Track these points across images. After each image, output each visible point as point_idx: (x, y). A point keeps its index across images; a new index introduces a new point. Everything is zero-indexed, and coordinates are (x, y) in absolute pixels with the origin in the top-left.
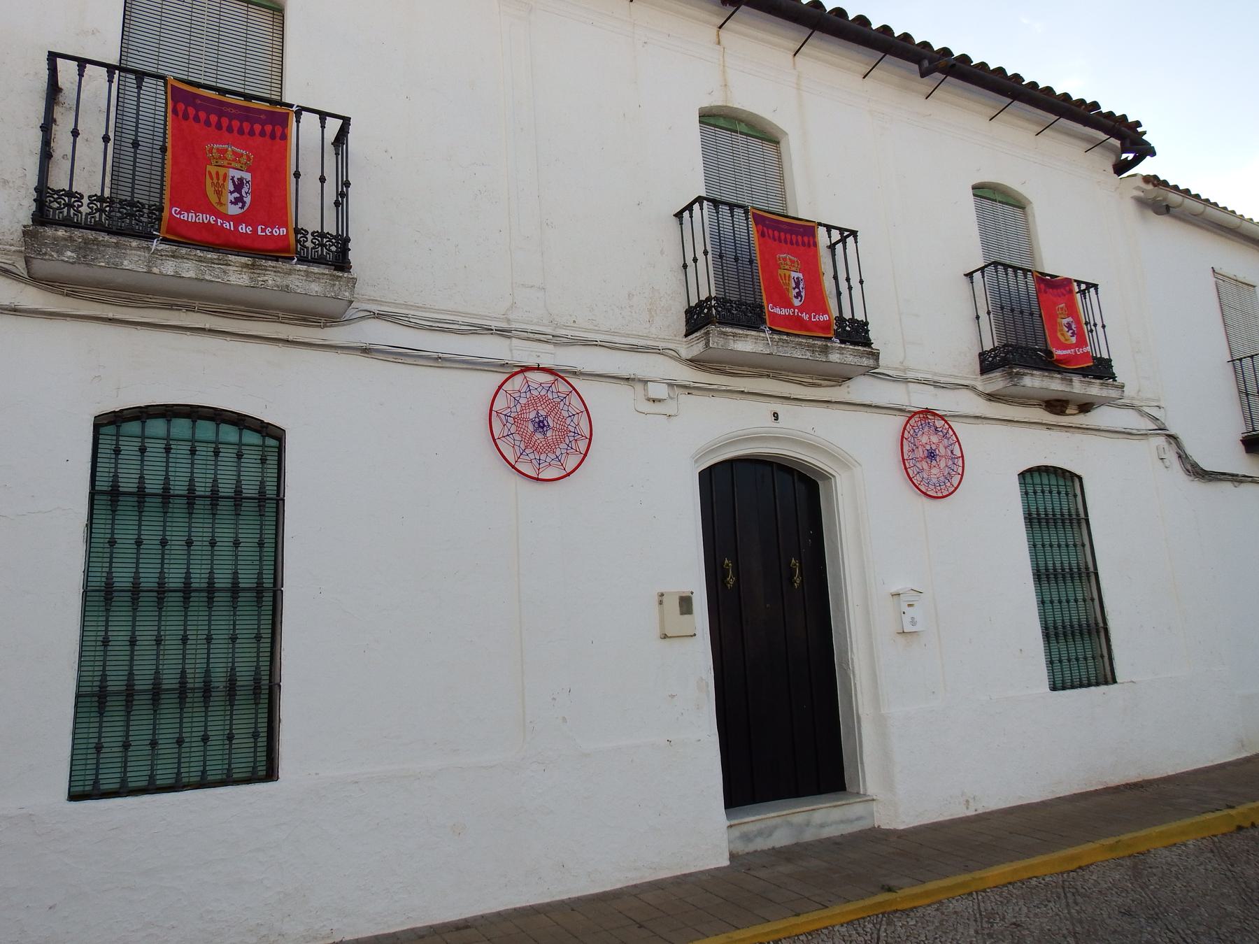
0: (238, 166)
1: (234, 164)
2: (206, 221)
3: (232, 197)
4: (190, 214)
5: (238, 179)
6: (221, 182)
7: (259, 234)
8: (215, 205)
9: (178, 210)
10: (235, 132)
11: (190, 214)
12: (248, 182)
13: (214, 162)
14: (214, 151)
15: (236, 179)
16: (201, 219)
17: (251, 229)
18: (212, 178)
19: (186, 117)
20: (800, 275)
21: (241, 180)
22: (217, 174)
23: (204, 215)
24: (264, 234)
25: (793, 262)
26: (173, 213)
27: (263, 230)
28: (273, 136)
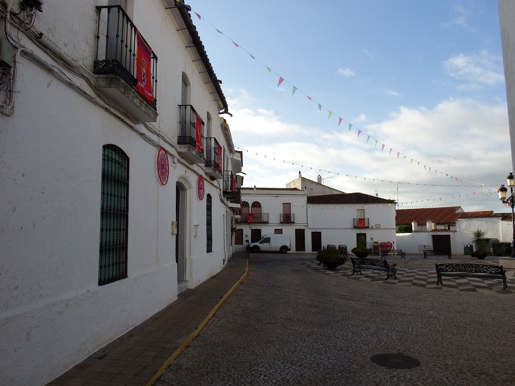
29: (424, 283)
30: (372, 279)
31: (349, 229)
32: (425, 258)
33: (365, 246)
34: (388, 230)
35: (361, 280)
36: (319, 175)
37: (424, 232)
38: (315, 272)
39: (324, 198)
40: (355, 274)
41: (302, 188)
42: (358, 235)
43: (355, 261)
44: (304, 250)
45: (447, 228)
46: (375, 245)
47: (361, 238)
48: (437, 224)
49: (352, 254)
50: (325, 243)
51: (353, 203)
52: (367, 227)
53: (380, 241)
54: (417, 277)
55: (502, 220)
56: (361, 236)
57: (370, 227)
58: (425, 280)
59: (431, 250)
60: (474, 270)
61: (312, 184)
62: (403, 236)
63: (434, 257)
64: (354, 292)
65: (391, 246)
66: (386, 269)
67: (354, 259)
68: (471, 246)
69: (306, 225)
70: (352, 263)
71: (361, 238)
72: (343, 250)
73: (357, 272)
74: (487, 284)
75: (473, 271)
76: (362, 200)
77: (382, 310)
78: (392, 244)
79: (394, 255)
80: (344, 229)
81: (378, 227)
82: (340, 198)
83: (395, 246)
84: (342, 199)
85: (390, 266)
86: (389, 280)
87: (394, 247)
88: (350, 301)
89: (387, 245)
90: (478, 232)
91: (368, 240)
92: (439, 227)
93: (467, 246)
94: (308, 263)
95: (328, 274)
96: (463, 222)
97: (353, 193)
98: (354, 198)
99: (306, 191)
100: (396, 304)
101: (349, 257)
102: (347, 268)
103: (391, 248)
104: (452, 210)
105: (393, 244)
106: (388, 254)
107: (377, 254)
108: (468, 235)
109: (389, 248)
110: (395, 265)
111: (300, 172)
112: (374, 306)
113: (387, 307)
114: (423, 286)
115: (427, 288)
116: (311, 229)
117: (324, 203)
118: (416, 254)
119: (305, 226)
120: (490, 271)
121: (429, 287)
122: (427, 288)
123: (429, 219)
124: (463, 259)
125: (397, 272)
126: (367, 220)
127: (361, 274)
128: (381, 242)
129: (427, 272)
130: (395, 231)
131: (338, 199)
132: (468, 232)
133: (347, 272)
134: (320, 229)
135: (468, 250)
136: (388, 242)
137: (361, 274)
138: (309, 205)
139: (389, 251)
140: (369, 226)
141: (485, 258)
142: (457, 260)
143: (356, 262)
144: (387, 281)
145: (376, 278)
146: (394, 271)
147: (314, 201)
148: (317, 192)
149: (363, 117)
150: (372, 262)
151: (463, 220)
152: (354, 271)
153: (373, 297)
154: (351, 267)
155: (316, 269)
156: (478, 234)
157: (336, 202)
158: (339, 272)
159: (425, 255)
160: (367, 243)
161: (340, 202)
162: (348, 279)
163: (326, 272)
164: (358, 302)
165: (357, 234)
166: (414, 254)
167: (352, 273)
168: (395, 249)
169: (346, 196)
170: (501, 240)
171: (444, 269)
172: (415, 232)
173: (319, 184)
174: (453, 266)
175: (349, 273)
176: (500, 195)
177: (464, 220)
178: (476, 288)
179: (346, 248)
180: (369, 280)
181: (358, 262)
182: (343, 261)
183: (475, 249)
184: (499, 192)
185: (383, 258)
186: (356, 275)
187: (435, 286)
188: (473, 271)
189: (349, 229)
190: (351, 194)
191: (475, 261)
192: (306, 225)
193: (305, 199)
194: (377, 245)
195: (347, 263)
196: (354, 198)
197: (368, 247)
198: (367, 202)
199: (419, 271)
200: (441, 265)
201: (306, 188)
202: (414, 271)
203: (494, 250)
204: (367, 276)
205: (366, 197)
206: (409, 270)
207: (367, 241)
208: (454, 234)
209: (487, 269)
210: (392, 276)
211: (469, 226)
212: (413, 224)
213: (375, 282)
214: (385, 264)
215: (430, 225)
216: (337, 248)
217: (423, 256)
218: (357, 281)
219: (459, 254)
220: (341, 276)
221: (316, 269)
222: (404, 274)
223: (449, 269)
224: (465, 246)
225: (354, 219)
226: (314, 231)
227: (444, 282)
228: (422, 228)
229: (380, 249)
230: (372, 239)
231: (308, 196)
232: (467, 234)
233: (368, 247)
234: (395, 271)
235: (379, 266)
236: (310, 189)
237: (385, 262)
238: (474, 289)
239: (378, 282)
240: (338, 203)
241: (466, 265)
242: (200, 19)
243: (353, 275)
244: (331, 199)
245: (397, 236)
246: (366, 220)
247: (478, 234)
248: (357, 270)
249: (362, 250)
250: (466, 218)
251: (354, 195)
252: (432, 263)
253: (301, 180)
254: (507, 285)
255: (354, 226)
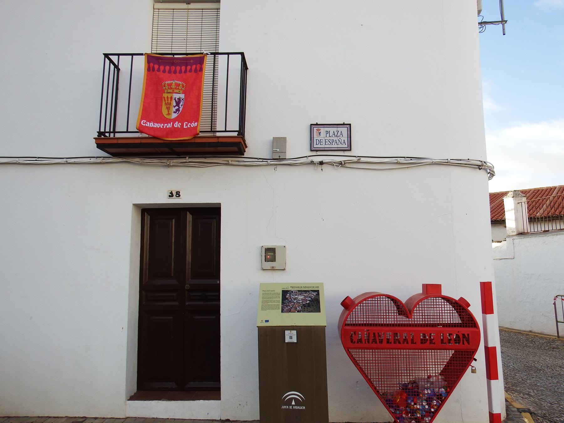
0: (177, 91)
1: (175, 91)
2: (158, 127)
3: (174, 110)
4: (151, 123)
5: (178, 99)
6: (169, 102)
7: (184, 127)
8: (165, 116)
9: (145, 121)
10: (161, 71)
11: (151, 123)
12: (183, 99)
13: (166, 91)
14: (166, 85)
15: (177, 99)
16: (177, 125)
17: (180, 124)
18: (165, 101)
19: (153, 70)
20: (182, 96)
21: (179, 99)
22: (168, 97)
23: (158, 124)
24: (187, 127)
25: (177, 85)
26: (143, 124)
27: (187, 125)
28: (196, 71)
46: (283, 329)
78: (476, 309)
89: (417, 317)
105: (487, 308)
128: (354, 293)
136: (344, 304)
140: (241, 131)
194: (300, 330)
242: (103, 54)
254: (429, 354)
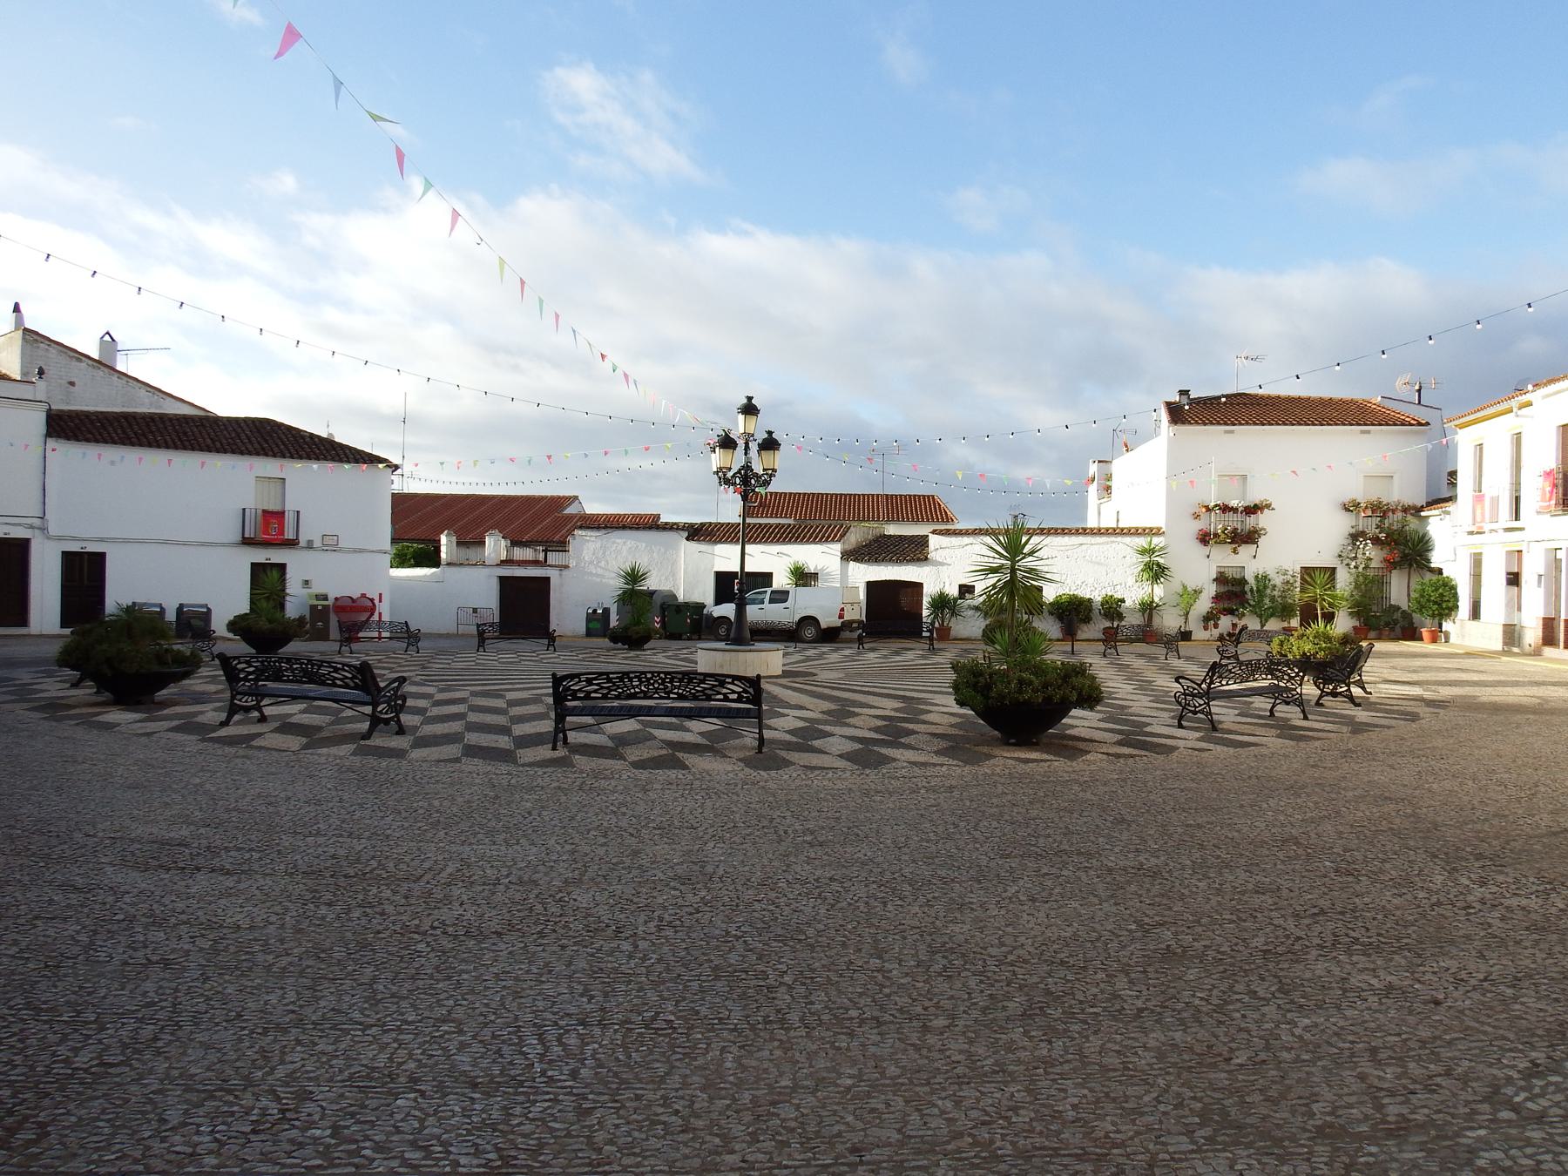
29: (503, 742)
30: (307, 737)
31: (223, 545)
32: (481, 649)
33: (282, 606)
34: (365, 555)
35: (260, 748)
36: (108, 333)
37: (476, 565)
38: (45, 718)
39: (125, 424)
40: (236, 718)
41: (24, 374)
42: (255, 567)
43: (240, 666)
44: (23, 620)
45: (541, 557)
47: (268, 581)
48: (515, 543)
49: (231, 635)
50: (119, 593)
51: (242, 453)
52: (292, 543)
53: (334, 592)
54: (473, 717)
55: (687, 539)
56: (269, 573)
57: (303, 543)
58: (505, 730)
59: (860, 622)
60: (675, 693)
61: (74, 363)
62: (409, 579)
63: (503, 644)
64: (226, 816)
65: (372, 610)
66: (368, 699)
67: (235, 658)
68: (606, 611)
69: (37, 522)
70: (221, 673)
71: (268, 581)
72: (194, 622)
73: (247, 710)
74: (698, 733)
75: (672, 696)
76: (277, 445)
77: (364, 921)
78: (376, 602)
79: (380, 638)
80: (203, 544)
81: (330, 545)
82: (192, 431)
83: (385, 611)
84: (200, 433)
85: (382, 685)
86: (377, 741)
87: (380, 614)
88: (199, 876)
90: (633, 570)
91: (293, 587)
92: (520, 553)
93: (595, 611)
94: (24, 676)
95: (109, 727)
96: (588, 541)
97: (246, 420)
98: (246, 435)
99: (41, 385)
100: (426, 865)
101: (217, 649)
102: (203, 693)
103: (372, 614)
104: (558, 503)
105: (380, 601)
106: (361, 635)
107: (323, 636)
108: (599, 580)
109: (363, 617)
110: (402, 680)
111: (17, 309)
112: (328, 897)
113: (388, 893)
114: (505, 756)
115: (523, 765)
116: (60, 539)
117: (124, 444)
118: (448, 636)
119: (31, 527)
120: (725, 694)
121: (527, 760)
122: (523, 765)
123: (492, 528)
124: (586, 648)
125: (410, 702)
126: (291, 520)
127: (263, 719)
129: (502, 697)
130: (388, 558)
131: (185, 433)
132: (600, 571)
133: (202, 713)
134: (102, 540)
135: (597, 623)
137: (263, 719)
138: (51, 443)
139: (364, 625)
141: (646, 646)
142: (572, 651)
143: (243, 670)
144: (367, 742)
145: (325, 734)
146: (398, 704)
147: (79, 429)
148: (93, 398)
149: (288, 182)
150: (311, 673)
151: (589, 533)
152: (233, 710)
153: (318, 833)
154: (220, 687)
155: (54, 708)
156: (634, 576)
157: (174, 443)
158: (165, 712)
159: (482, 638)
160: (288, 598)
161: (192, 445)
162: (201, 746)
163: (100, 718)
164: (239, 882)
165: (255, 567)
166: (440, 636)
167: (223, 716)
168: (386, 618)
169: (218, 426)
170: (681, 598)
171: (580, 690)
172: (449, 564)
173: (104, 365)
174: (609, 680)
175: (211, 714)
176: (717, 459)
177: (592, 534)
178: (680, 755)
179: (206, 616)
180: (294, 742)
181: (250, 673)
182: (188, 666)
183: (614, 621)
184: (714, 451)
185: (343, 648)
186: (238, 723)
187: (545, 752)
188: (672, 696)
189: (223, 545)
190: (237, 421)
191: (620, 660)
192: (37, 522)
193: (38, 420)
195: (204, 671)
196: (246, 435)
197: (292, 610)
198: (298, 453)
199: (474, 694)
200: (571, 677)
201: (41, 372)
202: (458, 695)
203: (663, 622)
204: (287, 727)
205: (293, 436)
206: (441, 691)
207: (288, 591)
208: (561, 575)
209: (716, 686)
210: (387, 722)
211: (604, 553)
212: (443, 539)
213: (319, 751)
214: (364, 677)
215: (495, 546)
216: (171, 616)
217: (476, 640)
218: (241, 752)
219: (569, 634)
220: (171, 734)
221: (54, 708)
222: (425, 710)
223: (595, 691)
224: (590, 611)
225: (244, 509)
226: (74, 547)
227: (573, 737)
228: (472, 554)
229: (334, 620)
230: (306, 582)
231: (53, 407)
232: (597, 575)
233: (292, 610)
234: (400, 702)
235: (340, 686)
236: (64, 382)
237: (364, 670)
238: (672, 758)
239: (334, 750)
240: (185, 448)
241: (653, 676)
243: (228, 725)
244: (154, 428)
245: (393, 578)
246: (289, 520)
247: (634, 576)
248: (246, 701)
249: (270, 621)
250: (598, 528)
251: (248, 426)
252: (504, 663)
253: (24, 339)
255: (243, 537)
